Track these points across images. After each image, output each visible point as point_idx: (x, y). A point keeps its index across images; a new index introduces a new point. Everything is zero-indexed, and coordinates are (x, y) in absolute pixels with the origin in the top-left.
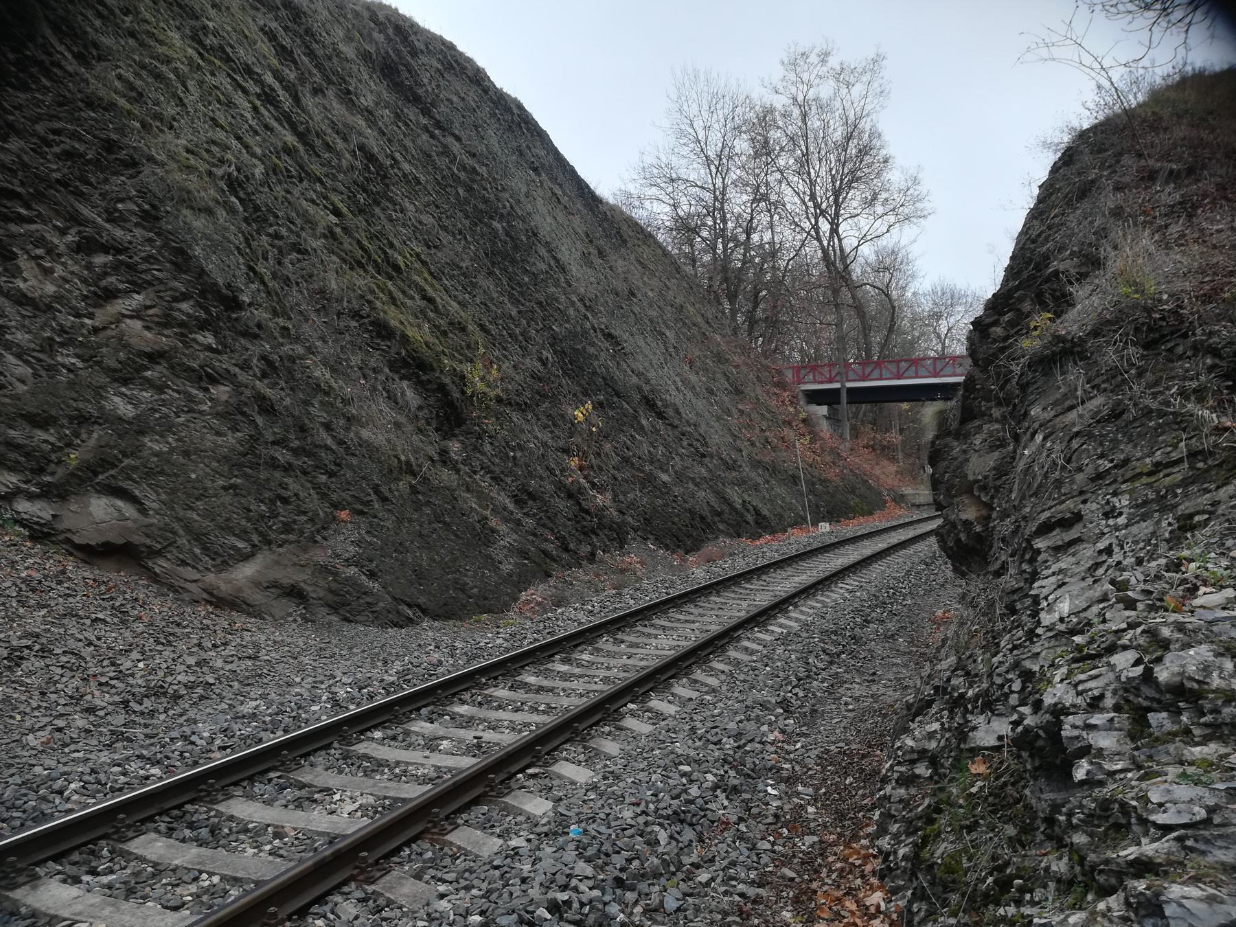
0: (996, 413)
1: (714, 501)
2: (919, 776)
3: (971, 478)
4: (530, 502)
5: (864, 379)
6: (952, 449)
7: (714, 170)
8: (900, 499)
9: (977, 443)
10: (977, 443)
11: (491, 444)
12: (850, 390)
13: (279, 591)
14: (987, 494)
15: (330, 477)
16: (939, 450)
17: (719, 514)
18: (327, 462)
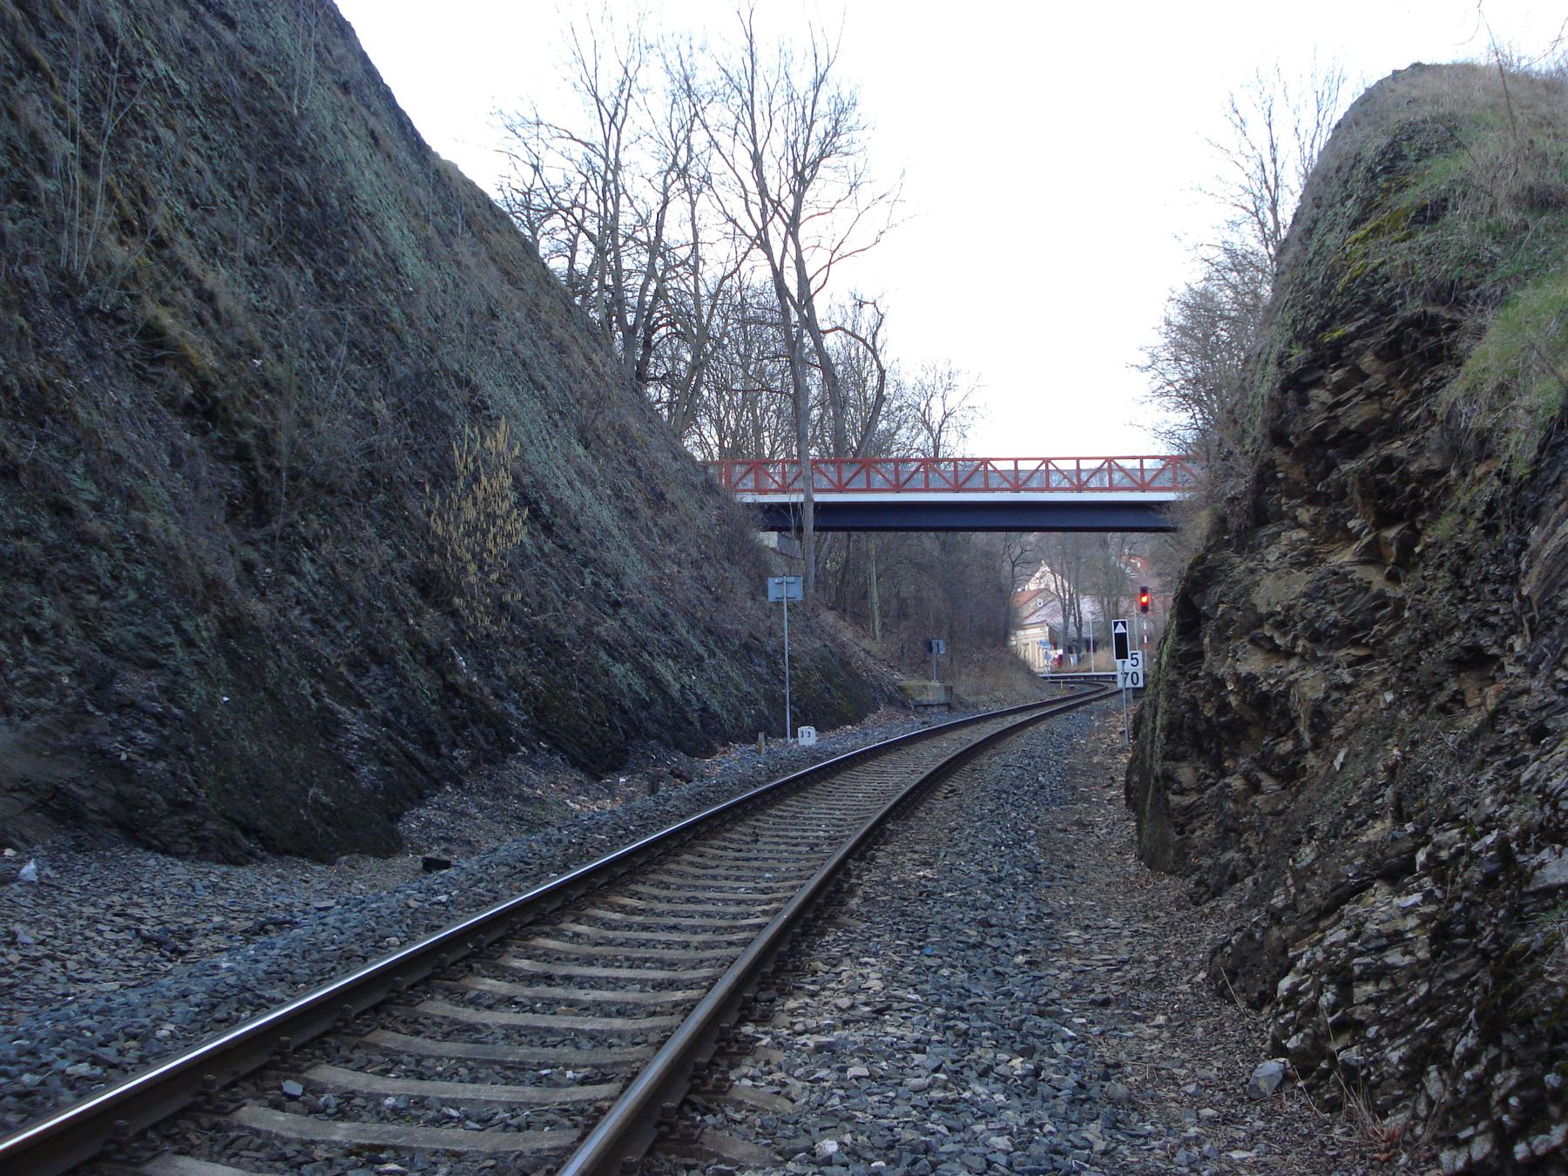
0: (1304, 515)
1: (638, 684)
2: (1392, 967)
3: (1263, 610)
4: (374, 669)
5: (841, 489)
6: (1233, 567)
7: (606, 119)
8: (901, 701)
9: (1272, 558)
10: (1272, 558)
11: (313, 561)
12: (822, 508)
13: (30, 800)
14: (1285, 634)
15: (102, 599)
16: (1213, 569)
17: (646, 706)
18: (100, 571)
